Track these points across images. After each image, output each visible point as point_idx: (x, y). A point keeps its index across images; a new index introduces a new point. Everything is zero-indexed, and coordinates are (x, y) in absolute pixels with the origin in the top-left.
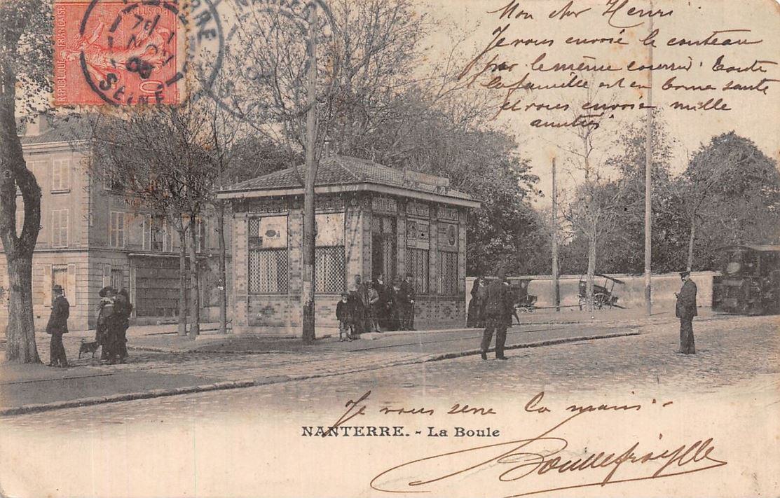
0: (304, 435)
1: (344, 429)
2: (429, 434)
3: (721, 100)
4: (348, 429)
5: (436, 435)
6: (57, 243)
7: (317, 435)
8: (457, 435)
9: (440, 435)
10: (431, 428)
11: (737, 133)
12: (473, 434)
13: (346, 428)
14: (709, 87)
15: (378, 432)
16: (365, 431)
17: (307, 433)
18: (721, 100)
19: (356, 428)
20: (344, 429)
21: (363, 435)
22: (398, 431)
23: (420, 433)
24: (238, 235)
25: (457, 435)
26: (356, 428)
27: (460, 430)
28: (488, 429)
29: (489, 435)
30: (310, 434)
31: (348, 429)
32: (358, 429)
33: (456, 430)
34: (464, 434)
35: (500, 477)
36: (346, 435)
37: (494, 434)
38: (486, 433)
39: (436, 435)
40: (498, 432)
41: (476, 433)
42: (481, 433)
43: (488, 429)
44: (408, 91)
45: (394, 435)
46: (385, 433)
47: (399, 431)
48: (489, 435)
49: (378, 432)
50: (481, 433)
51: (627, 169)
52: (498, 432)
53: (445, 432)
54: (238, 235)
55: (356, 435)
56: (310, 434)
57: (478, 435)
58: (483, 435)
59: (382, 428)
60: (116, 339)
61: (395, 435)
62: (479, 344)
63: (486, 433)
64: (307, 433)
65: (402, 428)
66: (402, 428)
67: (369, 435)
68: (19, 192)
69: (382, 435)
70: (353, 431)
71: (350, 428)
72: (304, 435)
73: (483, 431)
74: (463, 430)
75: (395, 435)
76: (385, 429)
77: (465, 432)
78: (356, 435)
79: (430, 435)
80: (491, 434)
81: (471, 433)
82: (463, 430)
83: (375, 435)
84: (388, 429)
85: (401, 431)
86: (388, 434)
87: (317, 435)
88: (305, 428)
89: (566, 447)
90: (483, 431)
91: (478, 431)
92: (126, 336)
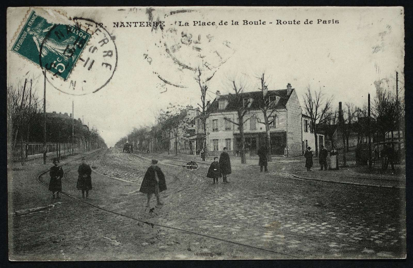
0: (114, 26)
3: (89, 69)
4: (136, 23)
5: (183, 25)
9: (185, 25)
10: (180, 22)
12: (249, 23)
13: (135, 23)
18: (89, 69)
19: (141, 23)
20: (134, 23)
23: (272, 23)
26: (141, 23)
28: (260, 21)
29: (260, 24)
31: (136, 23)
32: (142, 23)
33: (277, 21)
36: (136, 26)
37: (310, 23)
38: (259, 23)
39: (183, 25)
41: (254, 23)
42: (256, 23)
43: (260, 21)
45: (147, 26)
52: (265, 22)
53: (188, 23)
55: (141, 26)
58: (257, 24)
60: (335, 176)
62: (268, 165)
65: (164, 22)
66: (164, 22)
67: (147, 26)
69: (147, 26)
70: (139, 24)
71: (138, 23)
72: (114, 26)
73: (291, 22)
74: (247, 21)
76: (279, 21)
77: (248, 23)
78: (141, 26)
79: (180, 25)
80: (262, 23)
82: (281, 21)
85: (164, 24)
86: (150, 26)
87: (121, 26)
88: (115, 23)
90: (257, 22)
91: (255, 22)
92: (305, 159)
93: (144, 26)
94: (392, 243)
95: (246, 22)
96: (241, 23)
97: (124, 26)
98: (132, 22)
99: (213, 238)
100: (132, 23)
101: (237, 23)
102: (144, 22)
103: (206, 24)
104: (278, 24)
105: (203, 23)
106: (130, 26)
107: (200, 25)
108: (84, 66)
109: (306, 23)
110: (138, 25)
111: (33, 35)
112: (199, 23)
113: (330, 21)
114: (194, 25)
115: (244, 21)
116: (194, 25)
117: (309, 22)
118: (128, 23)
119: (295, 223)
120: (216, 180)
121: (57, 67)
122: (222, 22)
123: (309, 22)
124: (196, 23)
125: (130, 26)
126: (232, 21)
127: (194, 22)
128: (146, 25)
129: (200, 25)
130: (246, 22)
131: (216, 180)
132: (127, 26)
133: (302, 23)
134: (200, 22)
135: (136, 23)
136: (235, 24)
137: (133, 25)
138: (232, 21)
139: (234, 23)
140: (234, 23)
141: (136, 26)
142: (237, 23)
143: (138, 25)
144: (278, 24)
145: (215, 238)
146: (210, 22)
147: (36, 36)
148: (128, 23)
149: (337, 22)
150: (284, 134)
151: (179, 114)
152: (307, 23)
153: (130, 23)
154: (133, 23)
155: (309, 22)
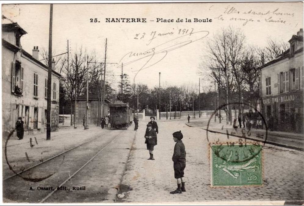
0: (107, 22)
1: (122, 19)
2: (186, 21)
6: (176, 181)
7: (112, 22)
8: (195, 22)
11: (21, 64)
12: (201, 21)
13: (123, 19)
14: (244, 20)
15: (136, 20)
16: (131, 20)
17: (108, 21)
19: (127, 19)
20: (122, 19)
21: (130, 22)
24: (78, 112)
25: (195, 22)
26: (127, 19)
27: (196, 19)
28: (207, 19)
29: (208, 21)
30: (109, 21)
33: (194, 20)
34: (197, 21)
36: (123, 21)
37: (209, 21)
38: (206, 21)
40: (173, 20)
41: (203, 21)
42: (204, 21)
46: (133, 21)
47: (129, 20)
48: (208, 21)
49: (136, 20)
50: (204, 21)
54: (78, 112)
55: (127, 22)
56: (109, 21)
57: (203, 22)
58: (205, 22)
59: (132, 19)
61: (143, 22)
64: (108, 21)
65: (146, 19)
66: (146, 19)
67: (132, 22)
69: (132, 22)
71: (125, 19)
75: (143, 22)
76: (133, 19)
77: (198, 20)
78: (127, 22)
80: (208, 21)
83: (135, 22)
84: (140, 19)
85: (146, 20)
86: (140, 21)
87: (112, 22)
88: (107, 19)
89: (208, 34)
90: (205, 20)
95: (196, 20)
96: (193, 20)
97: (114, 22)
99: (61, 71)
100: (120, 19)
101: (190, 21)
102: (130, 19)
103: (167, 21)
105: (164, 20)
106: (119, 21)
107: (162, 22)
109: (178, 21)
110: (111, 20)
111: (222, 168)
112: (161, 20)
114: (158, 22)
115: (195, 19)
116: (158, 22)
117: (180, 21)
118: (117, 19)
119: (80, 94)
124: (159, 19)
125: (119, 21)
126: (186, 19)
128: (142, 21)
129: (162, 22)
130: (196, 20)
132: (117, 22)
133: (175, 21)
134: (162, 19)
136: (188, 21)
137: (121, 21)
138: (186, 19)
139: (187, 21)
140: (187, 21)
141: (123, 21)
142: (190, 21)
143: (125, 21)
145: (61, 70)
146: (170, 20)
147: (224, 167)
148: (117, 19)
152: (179, 22)
153: (118, 19)
154: (121, 19)
155: (180, 21)
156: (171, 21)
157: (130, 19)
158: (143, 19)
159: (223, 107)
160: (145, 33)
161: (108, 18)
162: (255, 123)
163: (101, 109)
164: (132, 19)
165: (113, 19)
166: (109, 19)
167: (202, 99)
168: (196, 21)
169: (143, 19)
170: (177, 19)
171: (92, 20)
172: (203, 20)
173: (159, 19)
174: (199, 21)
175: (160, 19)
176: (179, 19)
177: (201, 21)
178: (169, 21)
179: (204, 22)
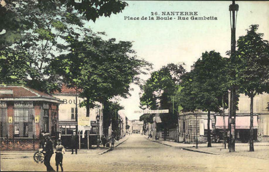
0: (163, 15)
12: (163, 19)
13: (177, 12)
17: (163, 14)
22: (171, 19)
26: (181, 12)
34: (159, 19)
35: (69, 103)
37: (137, 19)
38: (167, 18)
41: (164, 18)
44: (41, 115)
46: (179, 19)
48: (168, 19)
50: (166, 19)
51: (5, 103)
57: (165, 19)
58: (166, 19)
59: (186, 12)
63: (167, 18)
64: (163, 14)
65: (197, 12)
66: (197, 12)
68: (111, 125)
71: (179, 12)
77: (160, 18)
80: (130, 19)
81: (162, 19)
86: (188, 15)
88: (163, 13)
90: (166, 18)
93: (183, 15)
94: (71, 62)
98: (175, 12)
100: (175, 13)
101: (146, 18)
102: (183, 12)
103: (133, 19)
104: (179, 19)
108: (126, 119)
109: (142, 19)
110: (166, 13)
112: (128, 18)
113: (142, 19)
114: (125, 19)
118: (172, 12)
120: (75, 115)
121: (21, 86)
122: (143, 18)
123: (144, 18)
124: (126, 17)
127: (125, 17)
131: (75, 115)
132: (172, 15)
133: (140, 19)
134: (129, 17)
135: (178, 13)
139: (151, 19)
140: (151, 19)
144: (179, 19)
146: (135, 18)
148: (172, 12)
149: (216, 19)
150: (256, 130)
151: (148, 117)
153: (173, 13)
154: (176, 12)
156: (137, 19)
157: (183, 12)
158: (195, 12)
159: (22, 149)
160: (76, 28)
161: (164, 11)
162: (15, 74)
163: (12, 87)
164: (186, 12)
165: (168, 12)
166: (165, 12)
167: (26, 45)
168: (158, 19)
169: (195, 12)
170: (142, 17)
171: (153, 13)
172: (165, 18)
173: (126, 17)
174: (206, 18)
175: (128, 17)
176: (143, 17)
177: (163, 19)
178: (135, 19)
179: (142, 20)
